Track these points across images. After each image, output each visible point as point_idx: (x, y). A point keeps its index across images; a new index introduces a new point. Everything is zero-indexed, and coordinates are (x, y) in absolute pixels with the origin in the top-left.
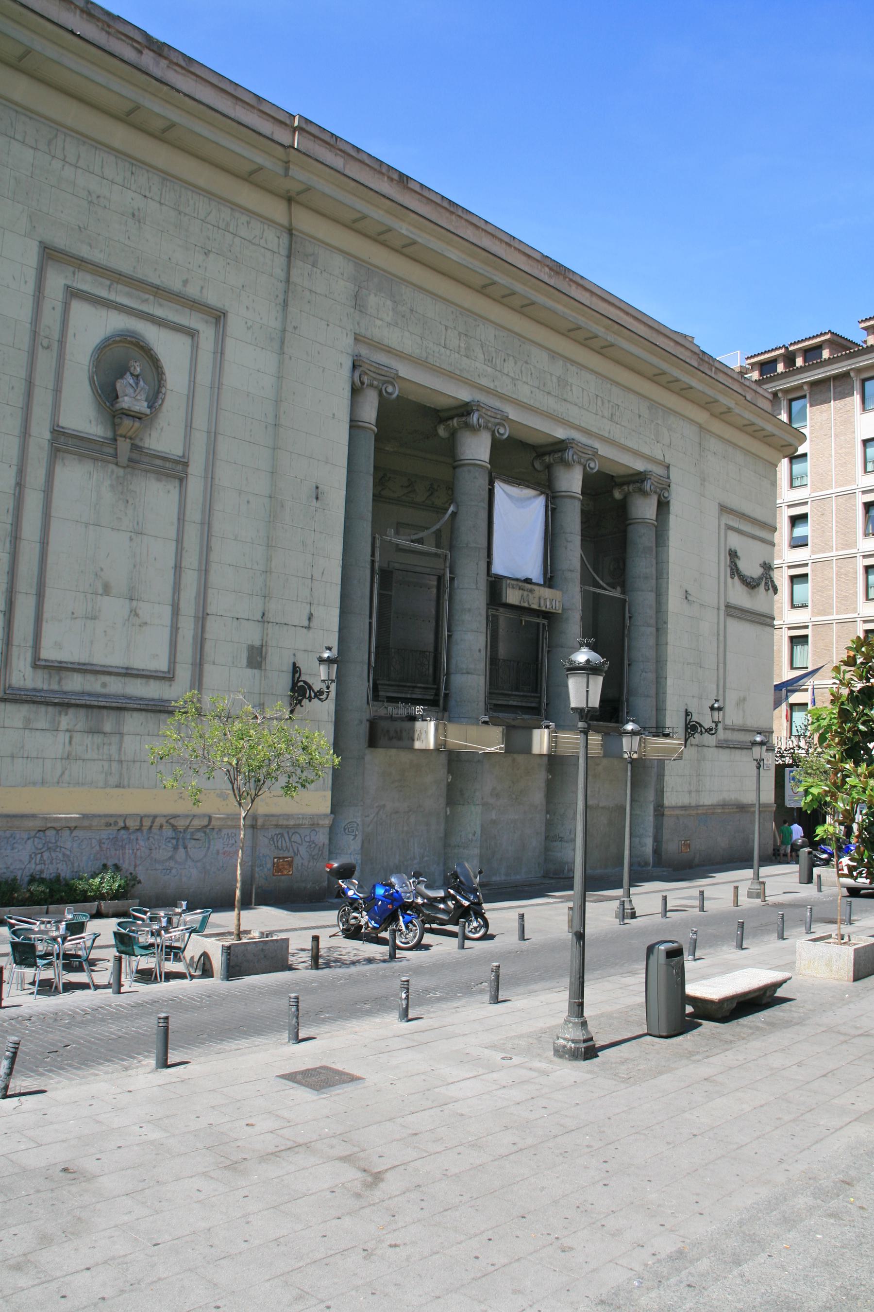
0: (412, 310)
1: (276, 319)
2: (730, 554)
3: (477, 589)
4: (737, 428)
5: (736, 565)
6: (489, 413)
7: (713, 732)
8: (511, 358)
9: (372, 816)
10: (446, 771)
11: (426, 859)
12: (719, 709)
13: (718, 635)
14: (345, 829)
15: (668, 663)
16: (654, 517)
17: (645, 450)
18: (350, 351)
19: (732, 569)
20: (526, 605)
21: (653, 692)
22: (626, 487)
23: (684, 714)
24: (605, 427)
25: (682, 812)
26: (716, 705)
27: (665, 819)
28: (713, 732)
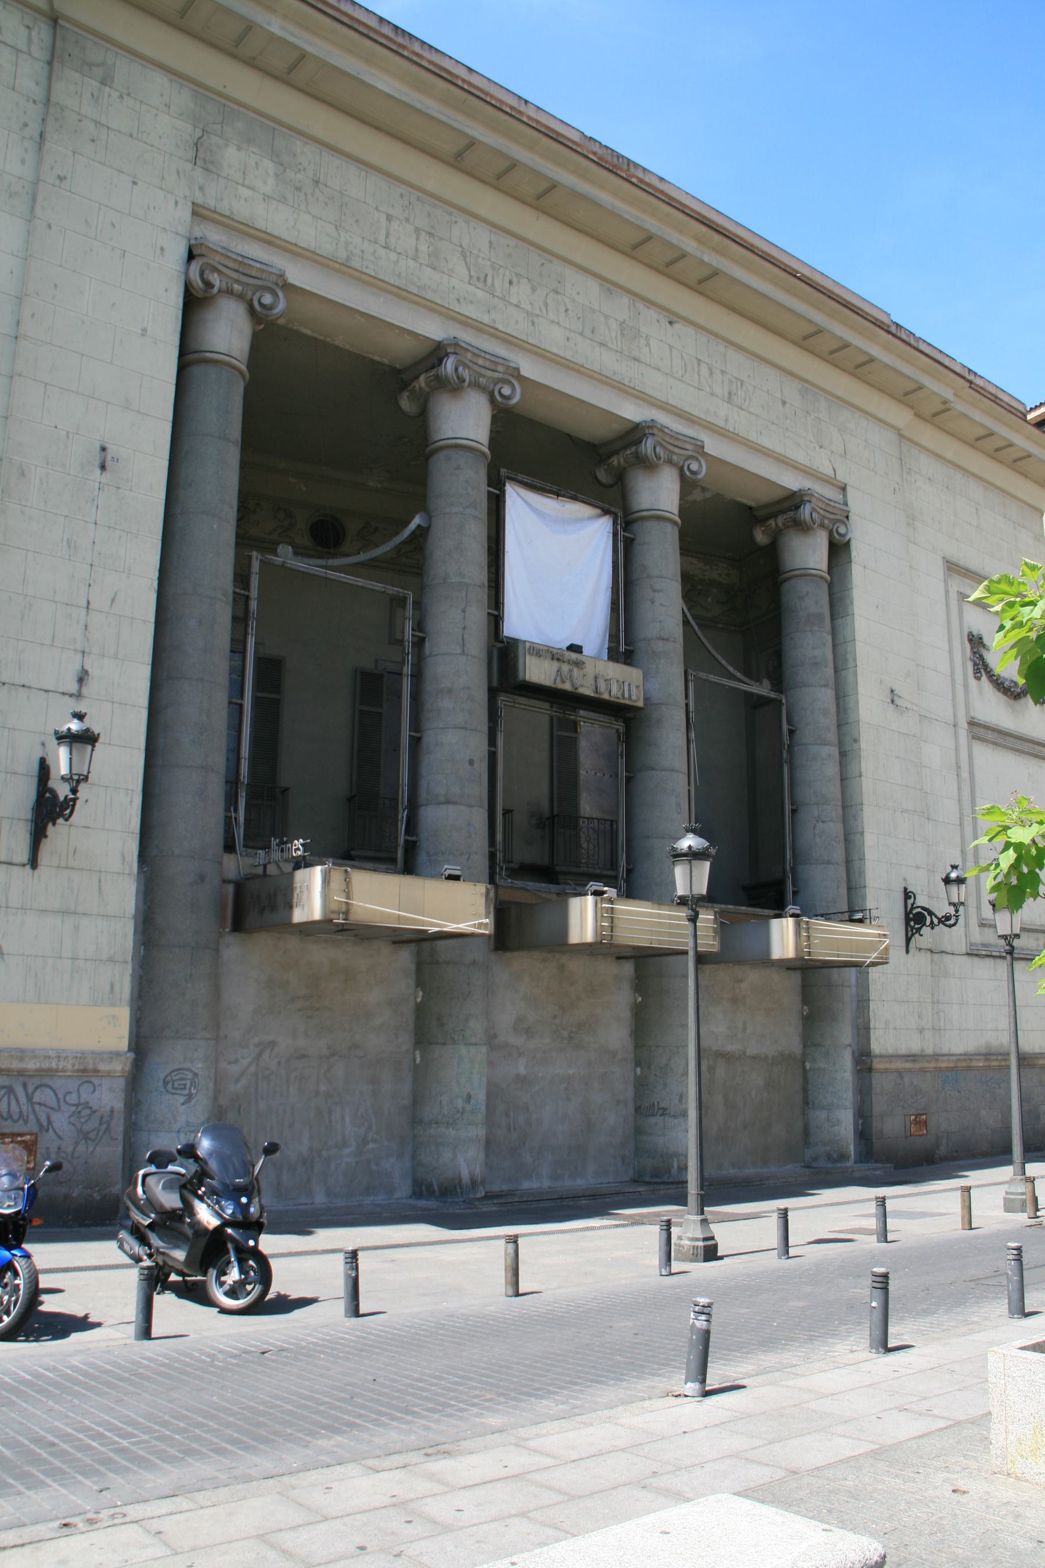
0: (317, 182)
1: (23, 162)
2: (970, 641)
3: (463, 653)
4: (966, 443)
5: (981, 658)
6: (480, 362)
7: (952, 922)
8: (525, 281)
9: (245, 1062)
10: (412, 982)
11: (371, 1146)
12: (960, 881)
13: (959, 767)
14: (165, 1083)
15: (865, 808)
16: (824, 566)
17: (799, 456)
18: (181, 230)
19: (975, 664)
20: (567, 687)
21: (839, 855)
22: (772, 522)
23: (901, 896)
24: (720, 413)
25: (909, 1065)
26: (953, 875)
27: (876, 1077)
28: (952, 922)
